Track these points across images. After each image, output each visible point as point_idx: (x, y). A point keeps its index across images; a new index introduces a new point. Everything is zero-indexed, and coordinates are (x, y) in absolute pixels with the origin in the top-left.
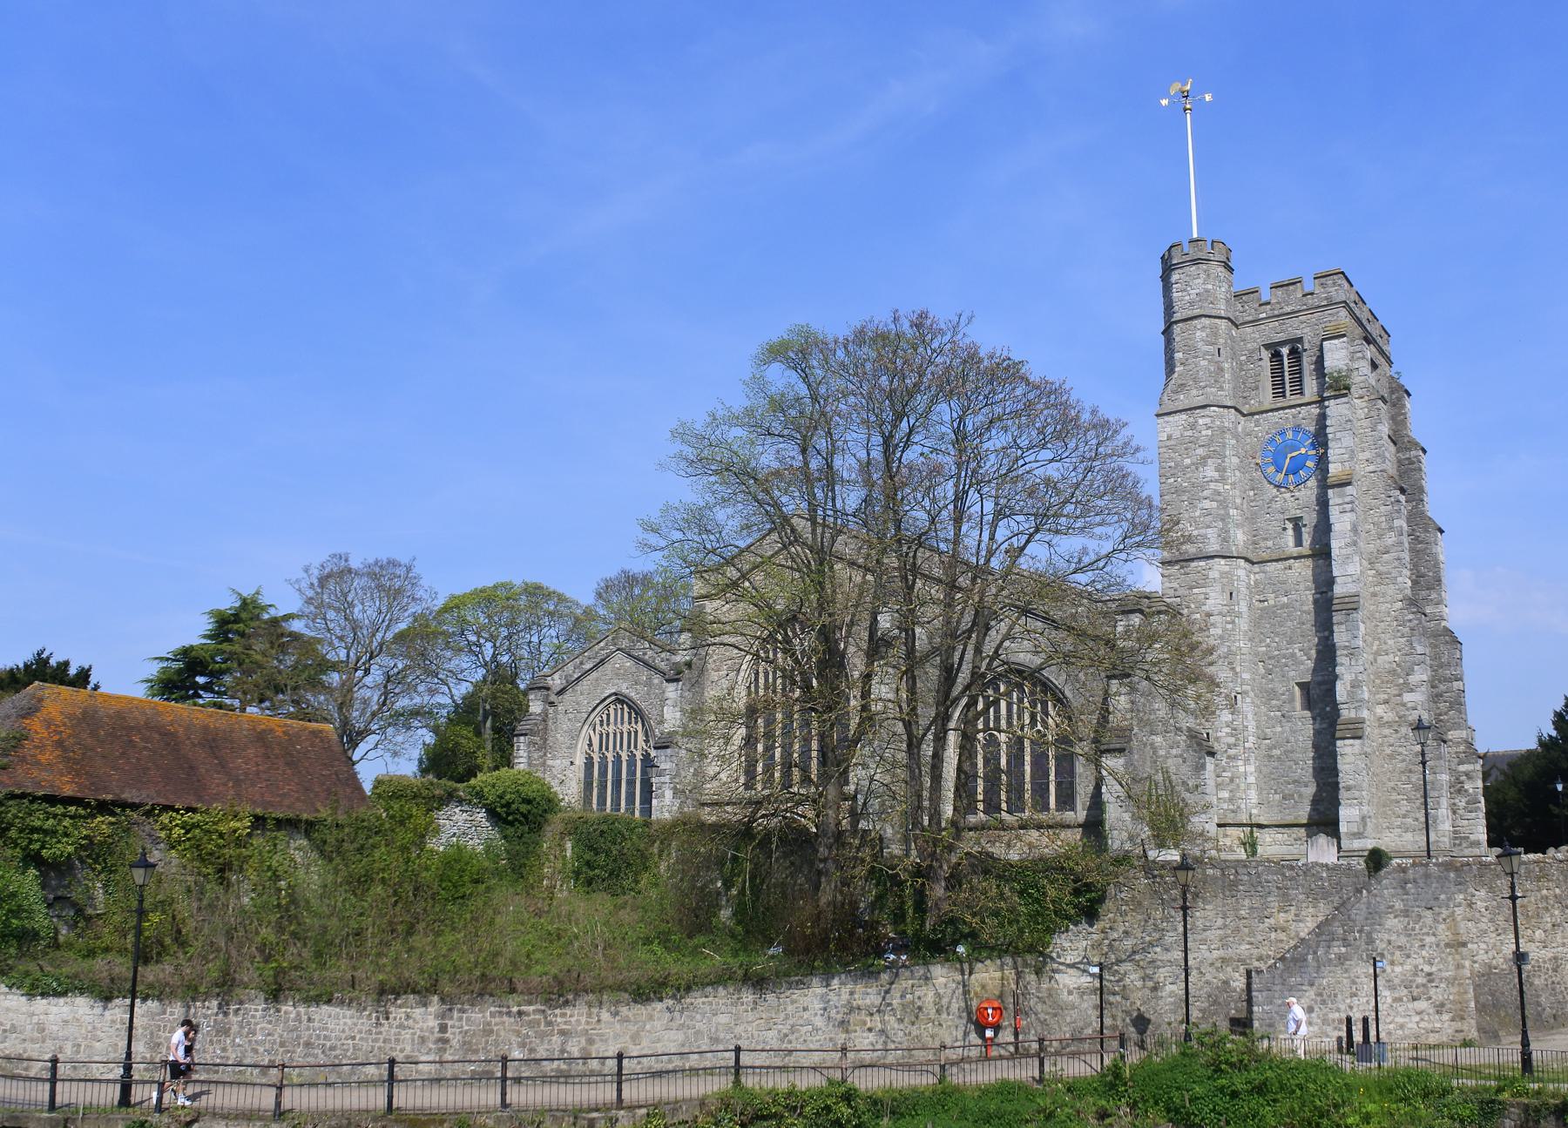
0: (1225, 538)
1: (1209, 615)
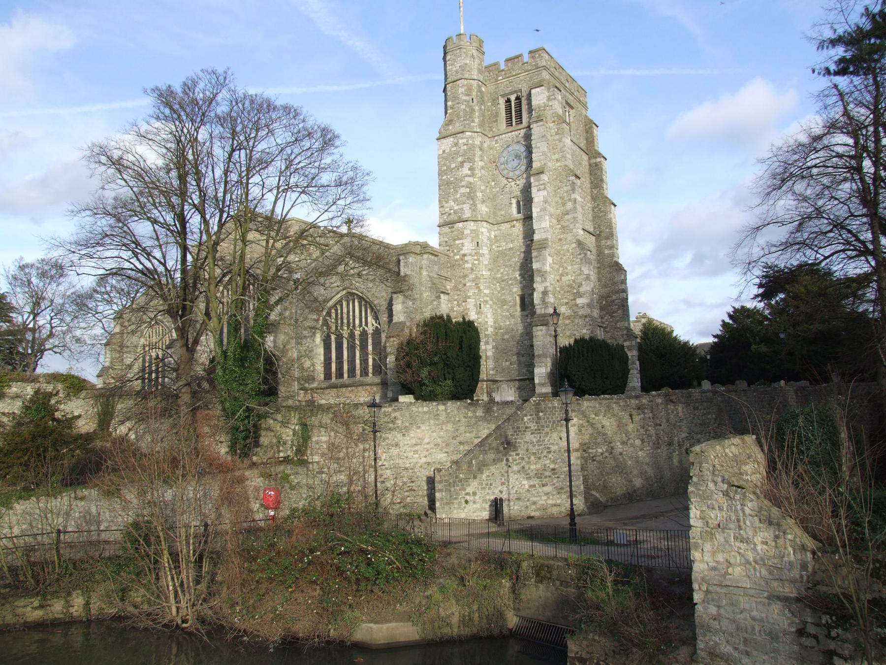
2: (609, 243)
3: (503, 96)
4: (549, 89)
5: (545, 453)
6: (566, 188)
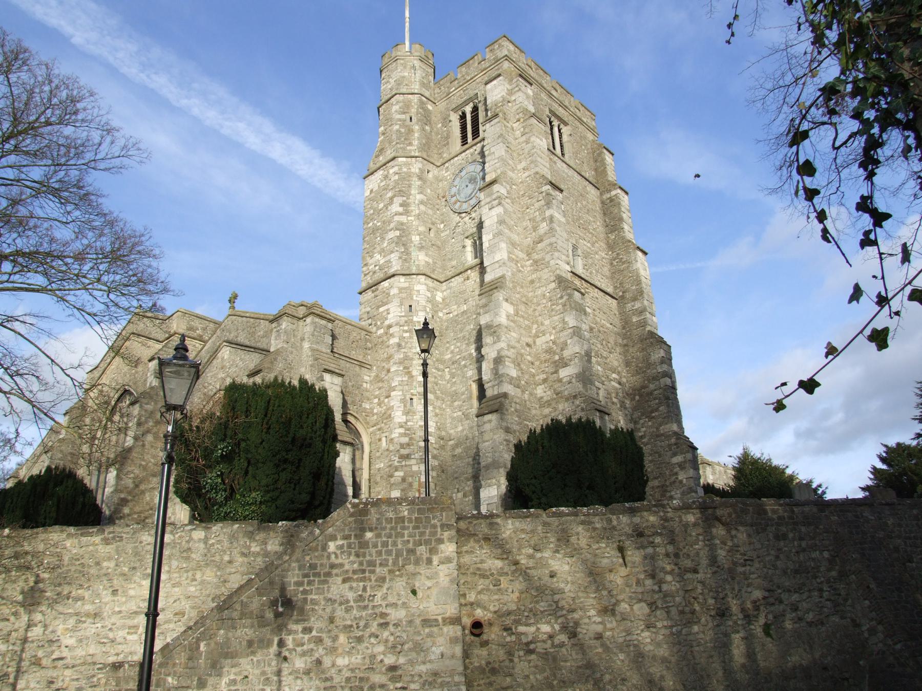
1: (390, 326)
2: (638, 305)
3: (455, 110)
4: (511, 81)
5: (374, 627)
6: (537, 205)
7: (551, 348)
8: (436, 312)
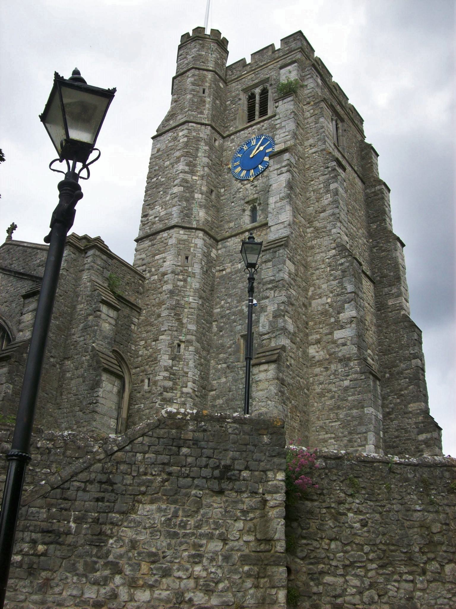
0: (187, 213)
1: (164, 274)
7: (327, 311)
8: (210, 267)
